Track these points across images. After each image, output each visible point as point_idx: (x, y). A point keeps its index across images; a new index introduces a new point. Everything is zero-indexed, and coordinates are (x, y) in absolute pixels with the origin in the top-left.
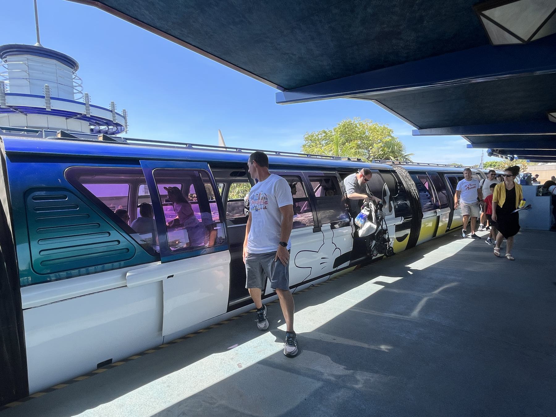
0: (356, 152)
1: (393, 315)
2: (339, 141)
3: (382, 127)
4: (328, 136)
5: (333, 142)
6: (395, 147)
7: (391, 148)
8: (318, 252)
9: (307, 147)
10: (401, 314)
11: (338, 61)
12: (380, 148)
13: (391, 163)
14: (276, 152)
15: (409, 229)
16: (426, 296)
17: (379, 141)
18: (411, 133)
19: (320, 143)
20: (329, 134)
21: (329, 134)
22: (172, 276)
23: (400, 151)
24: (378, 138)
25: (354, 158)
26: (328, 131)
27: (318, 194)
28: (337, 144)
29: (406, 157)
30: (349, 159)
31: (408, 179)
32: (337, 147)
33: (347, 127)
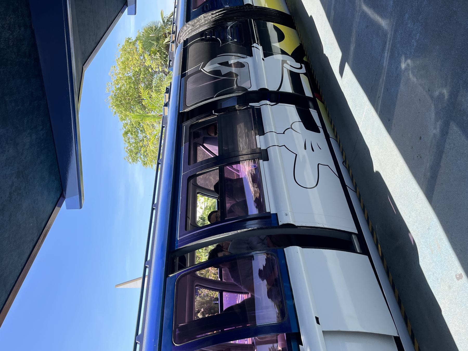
0: (155, 90)
1: (387, 54)
2: (140, 113)
3: (121, 52)
4: (132, 129)
5: (141, 122)
6: (150, 35)
7: (153, 42)
8: (296, 155)
9: (146, 159)
10: (386, 43)
11: (25, 121)
12: (151, 57)
13: (174, 45)
14: (153, 209)
15: (266, 24)
16: (360, 6)
17: (142, 58)
18: (132, 17)
19: (141, 141)
20: (129, 127)
21: (129, 127)
22: (317, 319)
23: (156, 29)
24: (138, 59)
25: (164, 98)
26: (125, 130)
27: (215, 150)
28: (144, 117)
29: (166, 21)
30: (166, 105)
31: (197, 23)
32: (148, 116)
33: (120, 101)
